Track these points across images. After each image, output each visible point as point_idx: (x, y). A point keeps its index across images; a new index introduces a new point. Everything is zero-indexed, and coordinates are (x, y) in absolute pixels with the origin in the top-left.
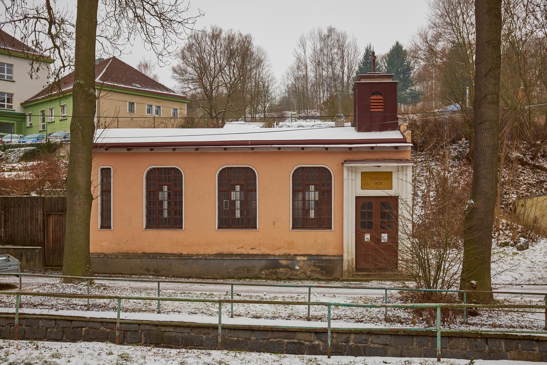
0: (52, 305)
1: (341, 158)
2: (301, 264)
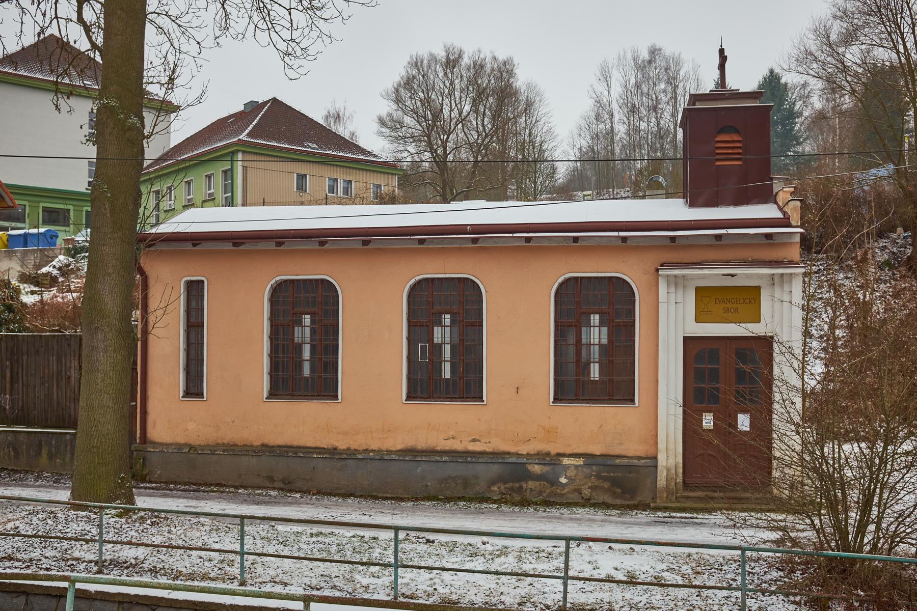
0: (31, 560)
1: (652, 259)
2: (571, 473)
